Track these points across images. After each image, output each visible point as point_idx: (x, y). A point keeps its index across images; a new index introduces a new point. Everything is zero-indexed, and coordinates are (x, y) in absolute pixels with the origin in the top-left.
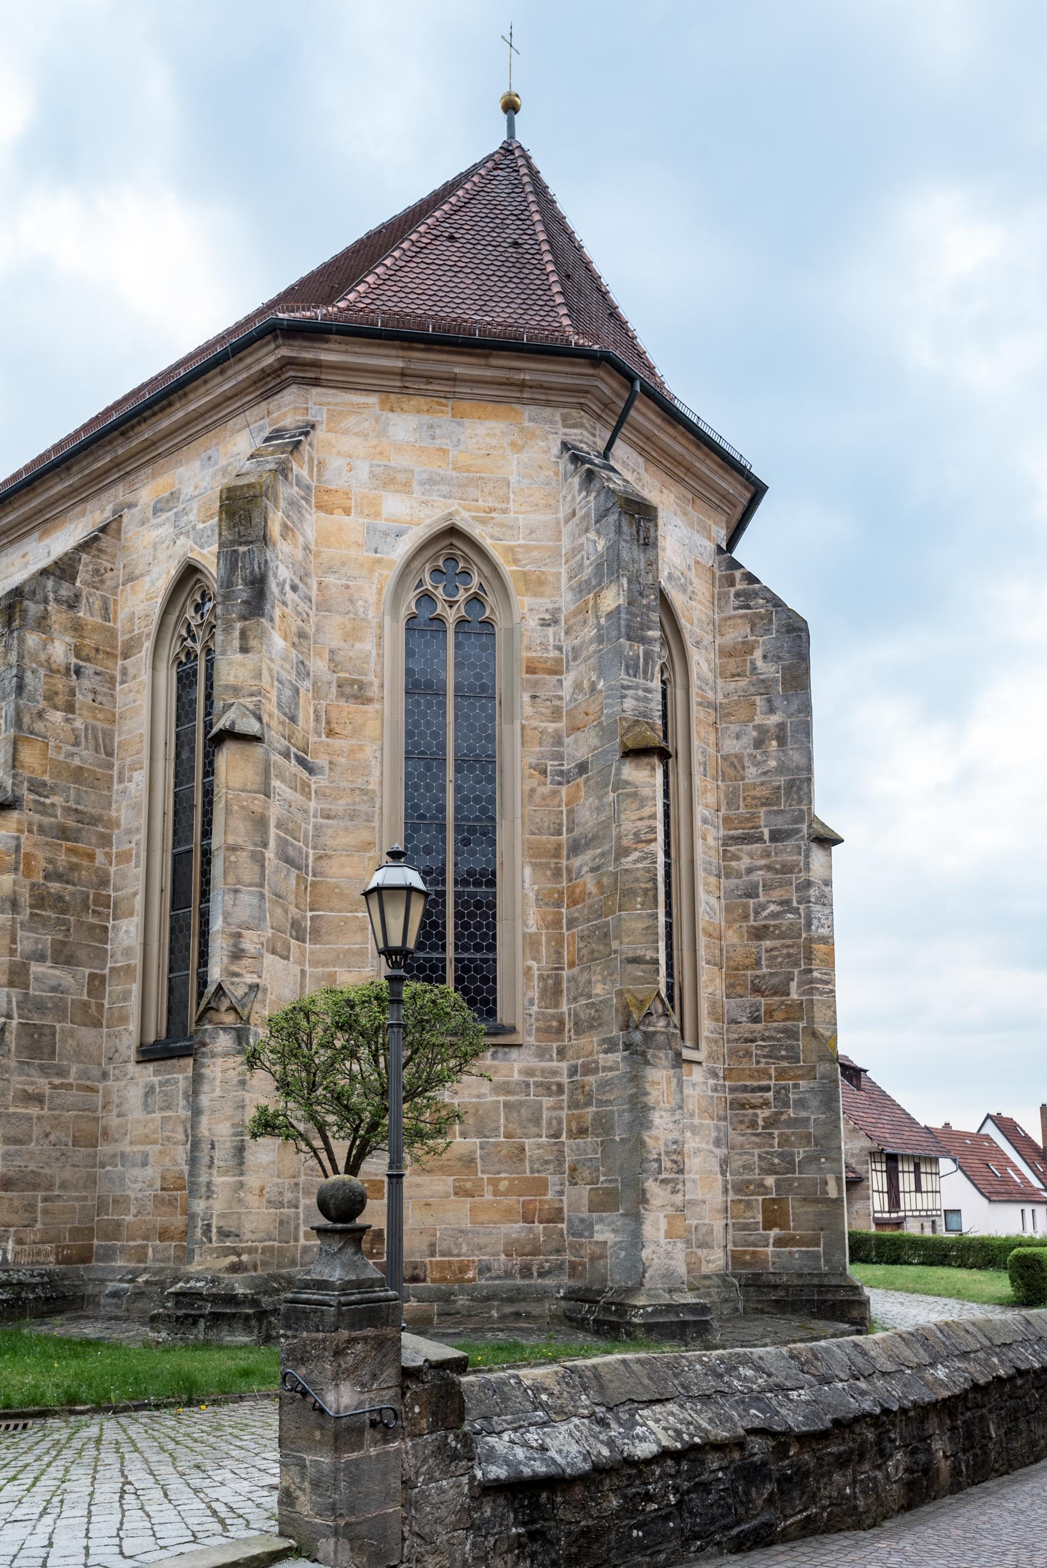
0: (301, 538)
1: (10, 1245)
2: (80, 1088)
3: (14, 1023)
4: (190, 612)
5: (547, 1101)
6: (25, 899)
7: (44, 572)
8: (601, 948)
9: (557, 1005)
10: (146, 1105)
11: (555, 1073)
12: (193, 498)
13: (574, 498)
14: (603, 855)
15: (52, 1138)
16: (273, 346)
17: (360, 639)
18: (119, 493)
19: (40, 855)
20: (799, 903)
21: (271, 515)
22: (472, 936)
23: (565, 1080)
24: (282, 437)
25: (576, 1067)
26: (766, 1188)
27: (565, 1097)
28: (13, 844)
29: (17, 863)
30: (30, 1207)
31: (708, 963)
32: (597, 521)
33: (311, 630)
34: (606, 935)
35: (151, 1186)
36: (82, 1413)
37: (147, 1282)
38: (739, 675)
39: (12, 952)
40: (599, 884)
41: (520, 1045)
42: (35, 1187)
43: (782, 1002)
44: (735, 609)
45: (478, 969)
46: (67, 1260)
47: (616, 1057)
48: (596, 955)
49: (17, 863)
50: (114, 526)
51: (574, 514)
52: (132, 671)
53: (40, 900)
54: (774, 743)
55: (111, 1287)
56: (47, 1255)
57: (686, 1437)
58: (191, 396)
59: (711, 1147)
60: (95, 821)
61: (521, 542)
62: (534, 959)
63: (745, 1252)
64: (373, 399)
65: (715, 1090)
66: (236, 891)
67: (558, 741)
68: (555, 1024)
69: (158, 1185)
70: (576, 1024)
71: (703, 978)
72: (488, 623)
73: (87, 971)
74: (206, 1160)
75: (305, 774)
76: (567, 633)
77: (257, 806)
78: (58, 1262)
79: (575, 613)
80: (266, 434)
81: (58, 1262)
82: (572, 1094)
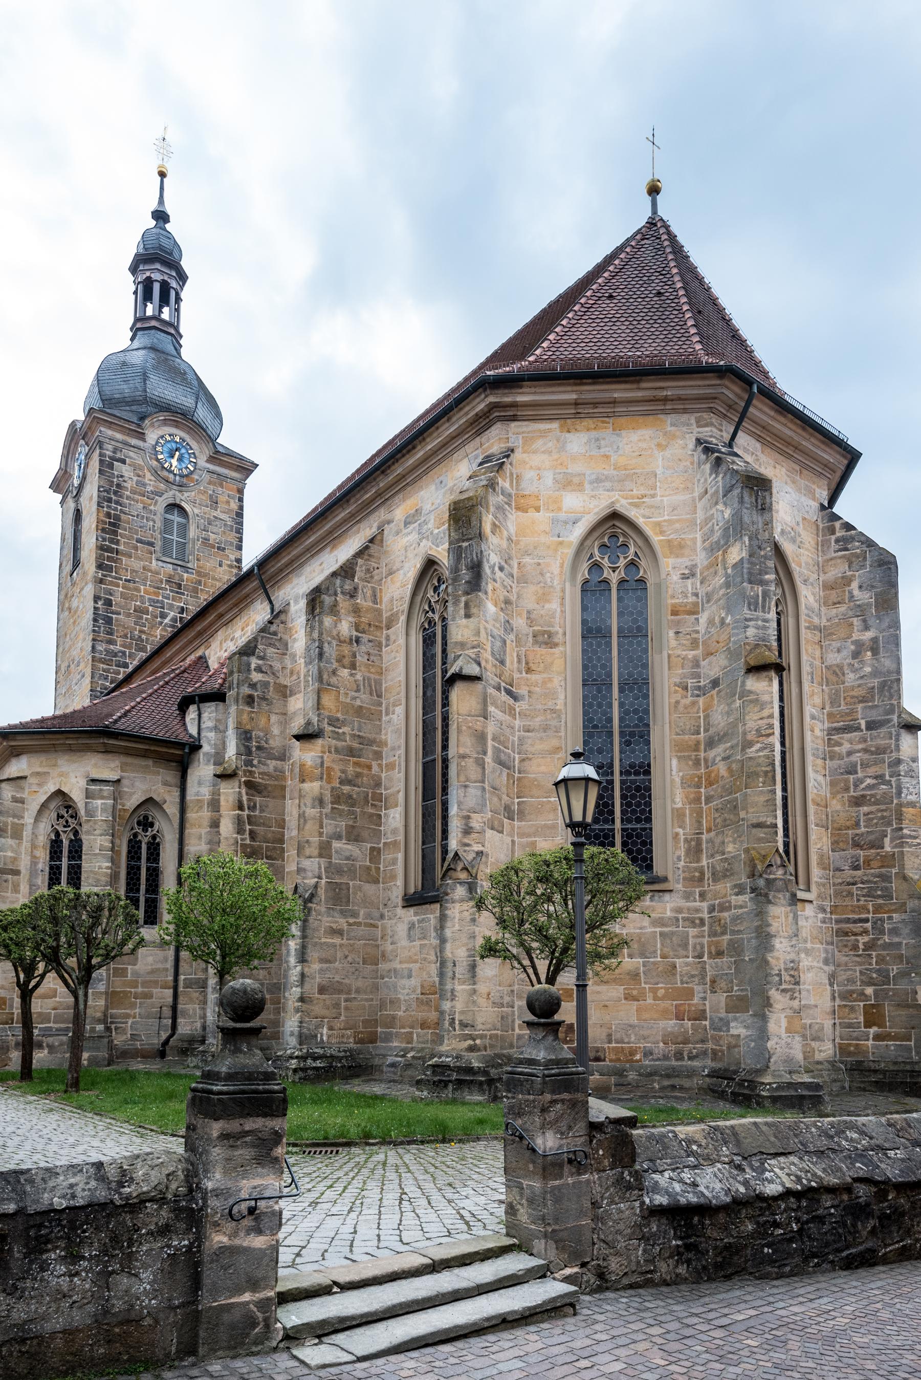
0: (505, 533)
1: (325, 1031)
2: (366, 925)
3: (323, 881)
4: (431, 593)
5: (692, 932)
6: (328, 798)
7: (334, 574)
8: (732, 817)
9: (698, 860)
10: (409, 936)
11: (697, 910)
12: (430, 512)
13: (706, 480)
14: (732, 747)
15: (349, 959)
16: (483, 396)
17: (549, 601)
18: (381, 515)
19: (337, 767)
20: (891, 776)
21: (484, 518)
22: (634, 812)
23: (706, 915)
24: (490, 461)
25: (714, 906)
26: (866, 996)
27: (706, 928)
28: (319, 761)
29: (322, 774)
30: (337, 1005)
31: (817, 825)
32: (724, 496)
33: (513, 598)
34: (735, 807)
35: (414, 991)
36: (373, 1144)
37: (413, 1057)
38: (839, 603)
39: (321, 834)
40: (730, 769)
41: (671, 891)
42: (340, 992)
43: (878, 854)
44: (835, 552)
45: (639, 836)
46: (361, 1041)
47: (745, 898)
48: (728, 822)
49: (322, 774)
50: (379, 537)
51: (706, 492)
52: (392, 638)
53: (337, 798)
54: (869, 653)
55: (390, 1060)
56: (348, 1038)
57: (805, 1181)
58: (428, 440)
59: (821, 965)
60: (371, 742)
61: (666, 518)
62: (680, 827)
63: (850, 1045)
64: (555, 425)
65: (824, 922)
66: (466, 786)
67: (696, 664)
68: (697, 874)
69: (419, 991)
70: (713, 874)
71: (813, 837)
72: (642, 581)
73: (369, 845)
74: (450, 974)
75: (511, 701)
76: (701, 583)
77: (479, 726)
78: (355, 1043)
79: (708, 568)
80: (480, 460)
81: (355, 1043)
82: (711, 926)
